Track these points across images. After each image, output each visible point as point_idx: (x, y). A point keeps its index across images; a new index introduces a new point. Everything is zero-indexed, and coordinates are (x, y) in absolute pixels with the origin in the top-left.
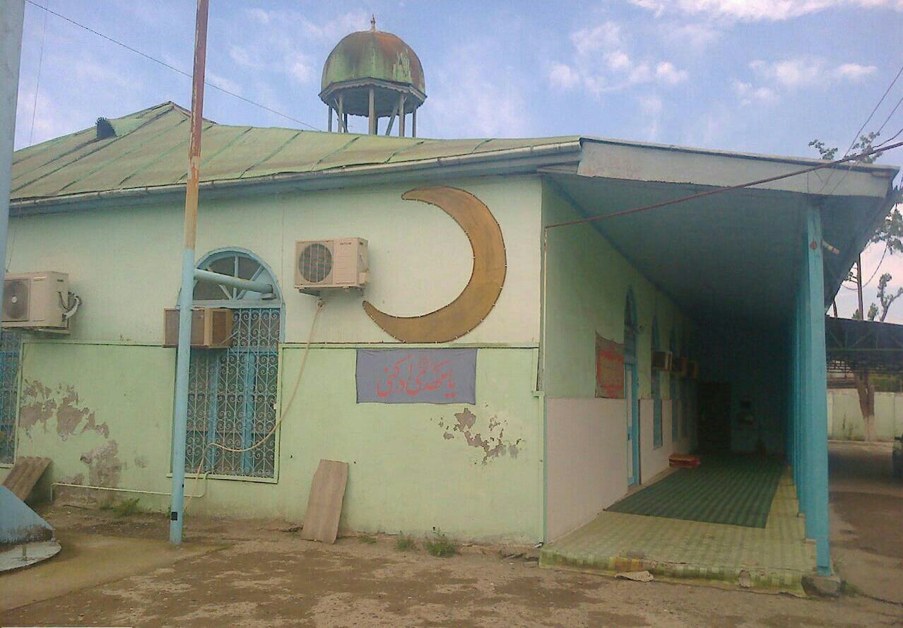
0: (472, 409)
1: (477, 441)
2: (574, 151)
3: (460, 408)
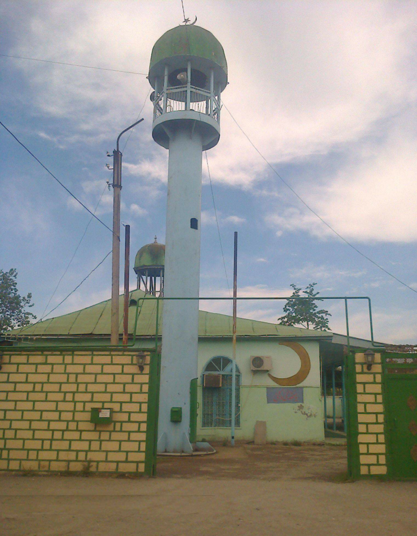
0: (303, 405)
1: (305, 414)
2: (332, 336)
3: (299, 404)
